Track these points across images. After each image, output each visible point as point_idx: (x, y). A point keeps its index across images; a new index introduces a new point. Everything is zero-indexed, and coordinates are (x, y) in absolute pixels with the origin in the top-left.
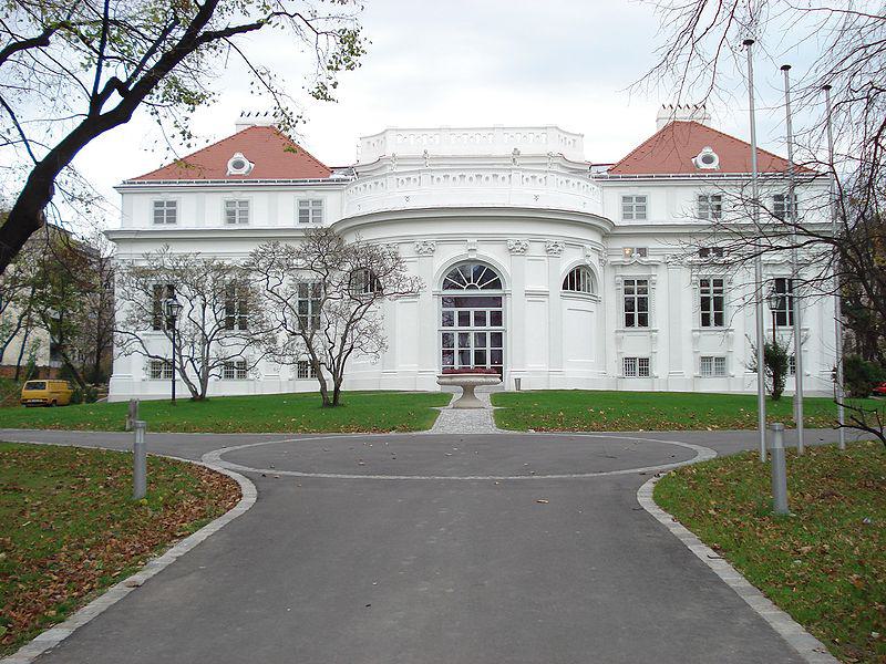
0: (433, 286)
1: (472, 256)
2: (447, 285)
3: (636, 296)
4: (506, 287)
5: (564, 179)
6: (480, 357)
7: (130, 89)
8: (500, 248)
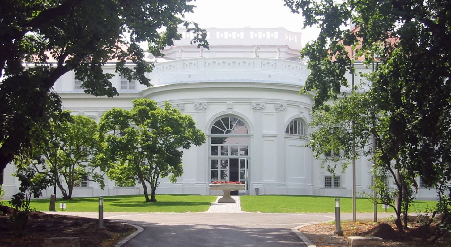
1: (230, 112)
7: (290, 177)
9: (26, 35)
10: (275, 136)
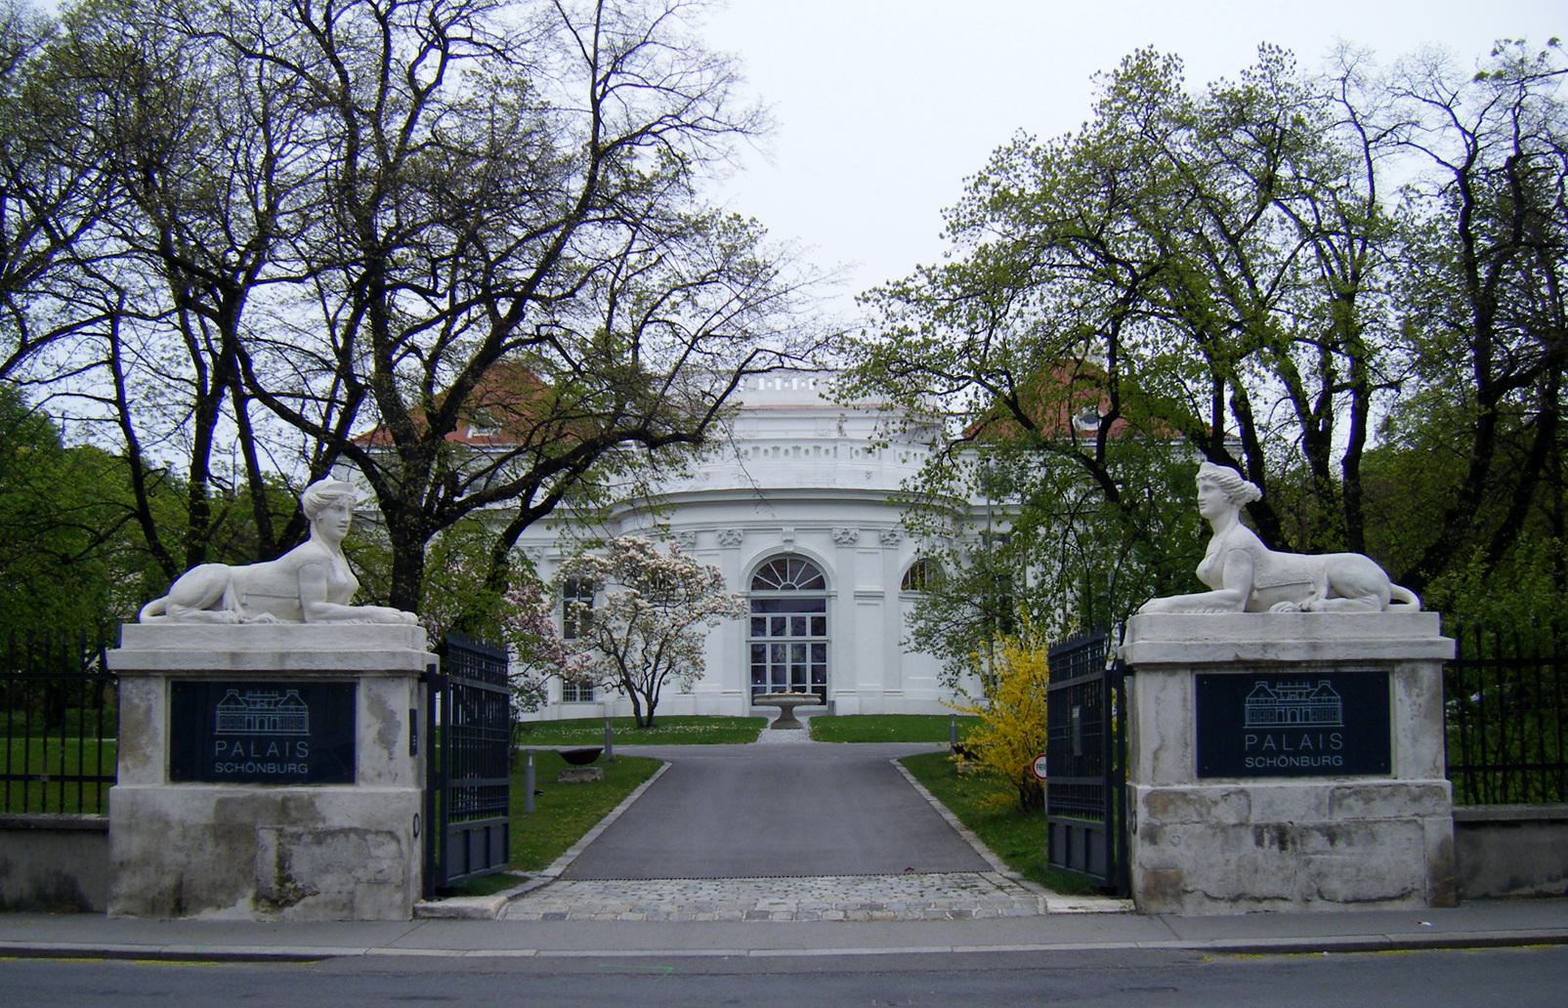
0: (737, 585)
1: (789, 549)
2: (757, 584)
4: (832, 587)
6: (798, 675)
8: (823, 538)
9: (1364, 450)
10: (880, 596)
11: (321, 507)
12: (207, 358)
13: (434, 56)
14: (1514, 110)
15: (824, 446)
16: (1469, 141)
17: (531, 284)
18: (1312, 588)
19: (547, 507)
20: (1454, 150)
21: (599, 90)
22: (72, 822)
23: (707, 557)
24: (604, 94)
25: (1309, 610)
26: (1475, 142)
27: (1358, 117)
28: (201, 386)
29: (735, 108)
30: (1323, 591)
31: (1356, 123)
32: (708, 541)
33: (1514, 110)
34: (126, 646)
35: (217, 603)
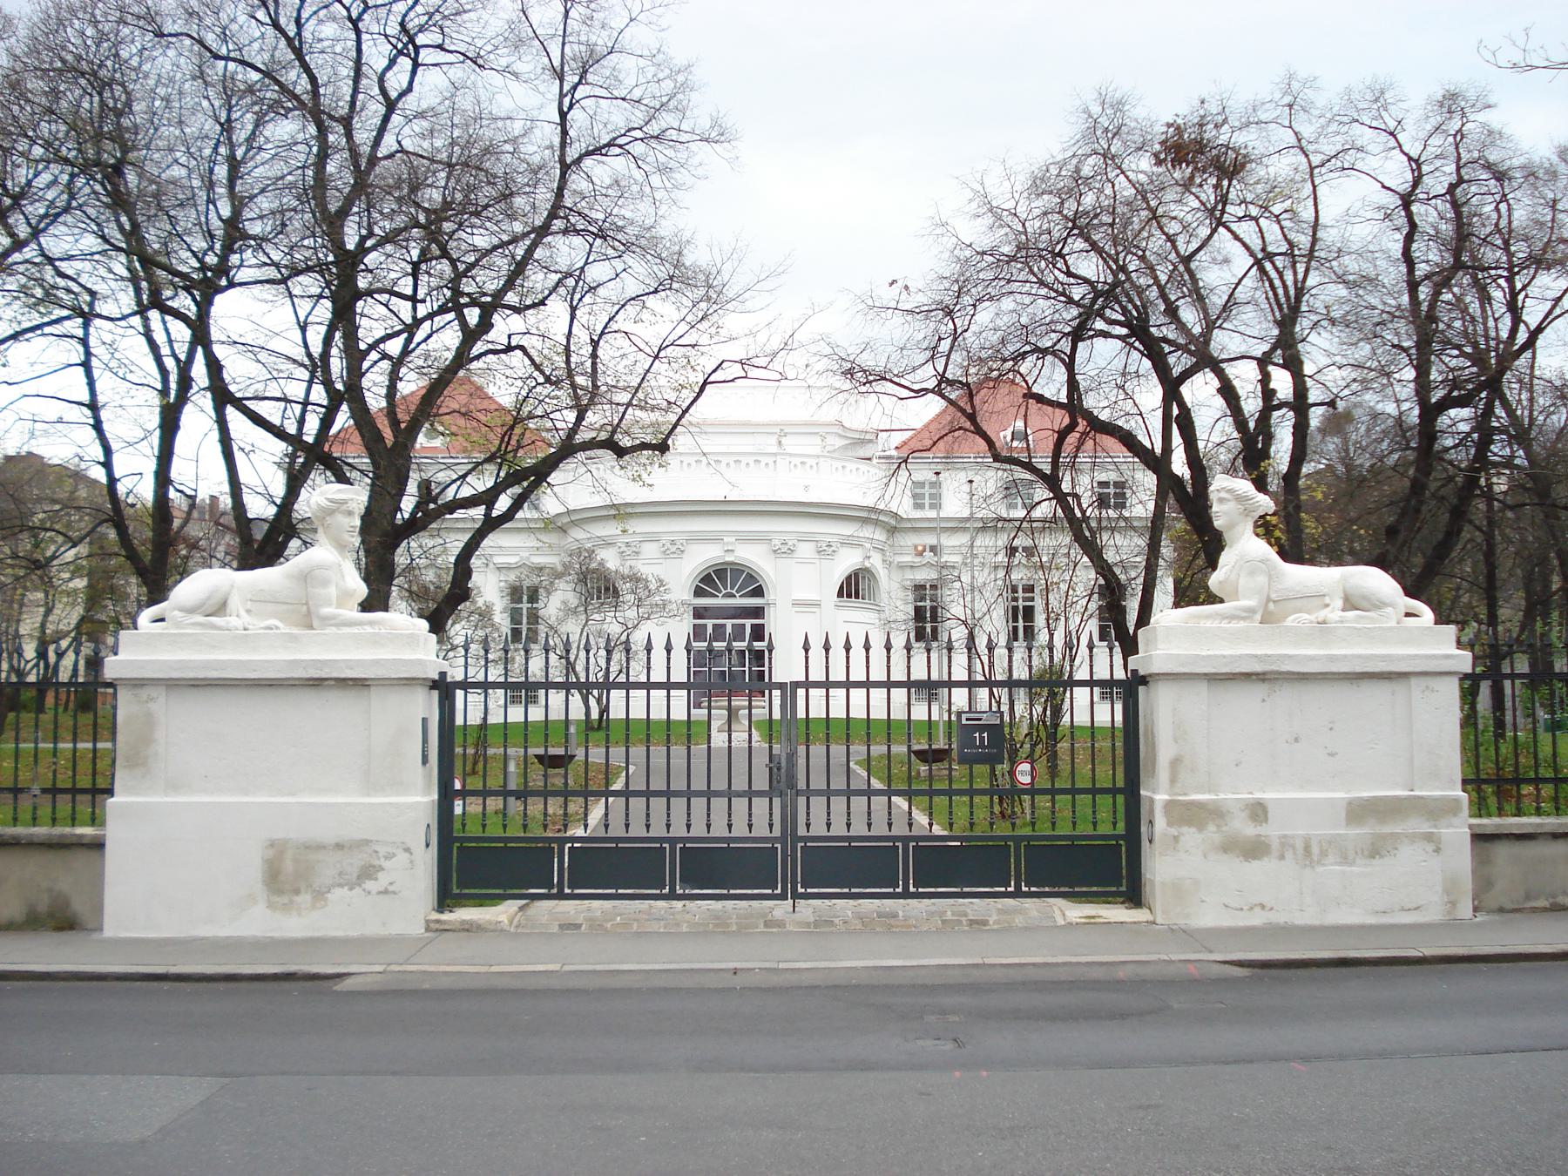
1: (729, 558)
2: (699, 592)
3: (1021, 603)
4: (771, 595)
5: (839, 464)
11: (331, 512)
12: (170, 363)
13: (405, 63)
14: (1455, 136)
15: (764, 460)
16: (1414, 166)
17: (499, 294)
18: (1327, 600)
19: (509, 515)
20: (1400, 177)
21: (567, 101)
22: (63, 836)
23: (649, 565)
24: (571, 107)
25: (1324, 622)
26: (1419, 168)
27: (1304, 143)
28: (164, 392)
29: (699, 118)
30: (1339, 603)
31: (1302, 149)
32: (650, 550)
33: (1455, 136)
34: (123, 655)
35: (221, 608)
